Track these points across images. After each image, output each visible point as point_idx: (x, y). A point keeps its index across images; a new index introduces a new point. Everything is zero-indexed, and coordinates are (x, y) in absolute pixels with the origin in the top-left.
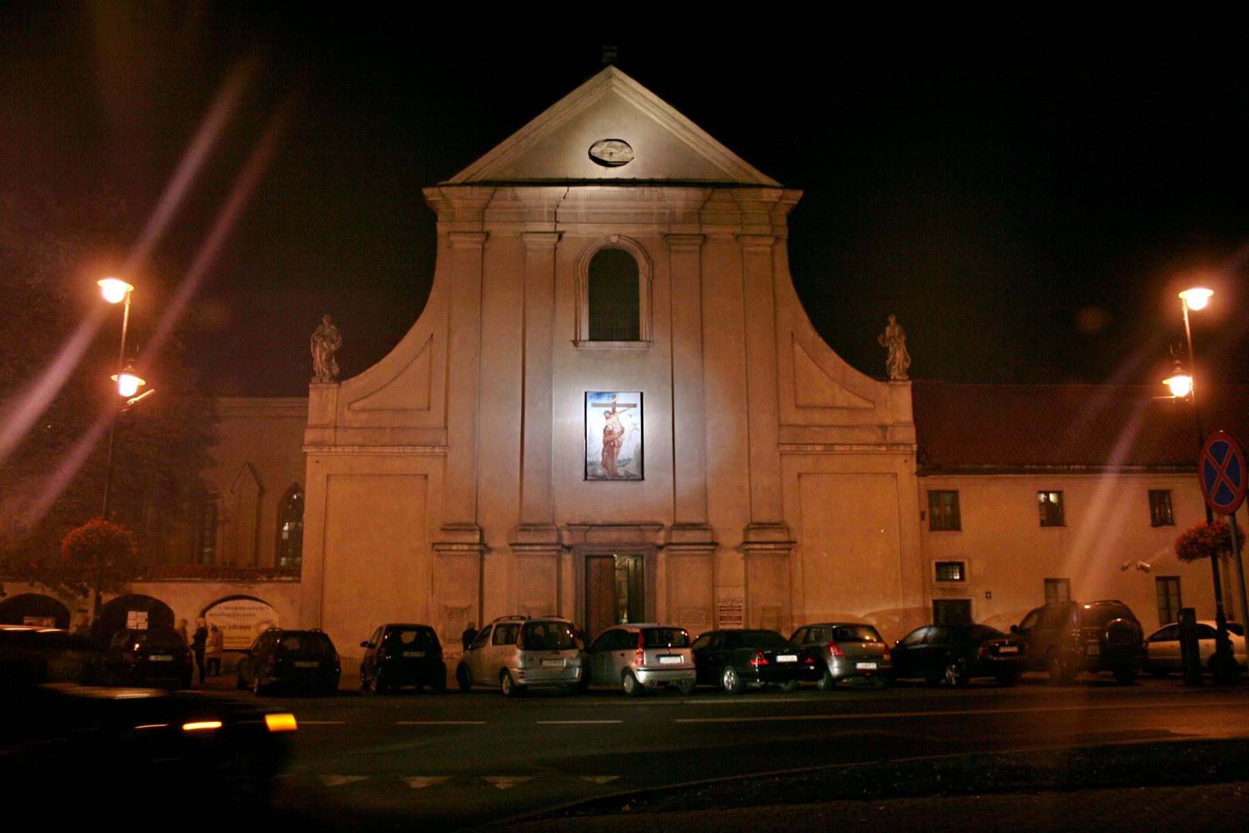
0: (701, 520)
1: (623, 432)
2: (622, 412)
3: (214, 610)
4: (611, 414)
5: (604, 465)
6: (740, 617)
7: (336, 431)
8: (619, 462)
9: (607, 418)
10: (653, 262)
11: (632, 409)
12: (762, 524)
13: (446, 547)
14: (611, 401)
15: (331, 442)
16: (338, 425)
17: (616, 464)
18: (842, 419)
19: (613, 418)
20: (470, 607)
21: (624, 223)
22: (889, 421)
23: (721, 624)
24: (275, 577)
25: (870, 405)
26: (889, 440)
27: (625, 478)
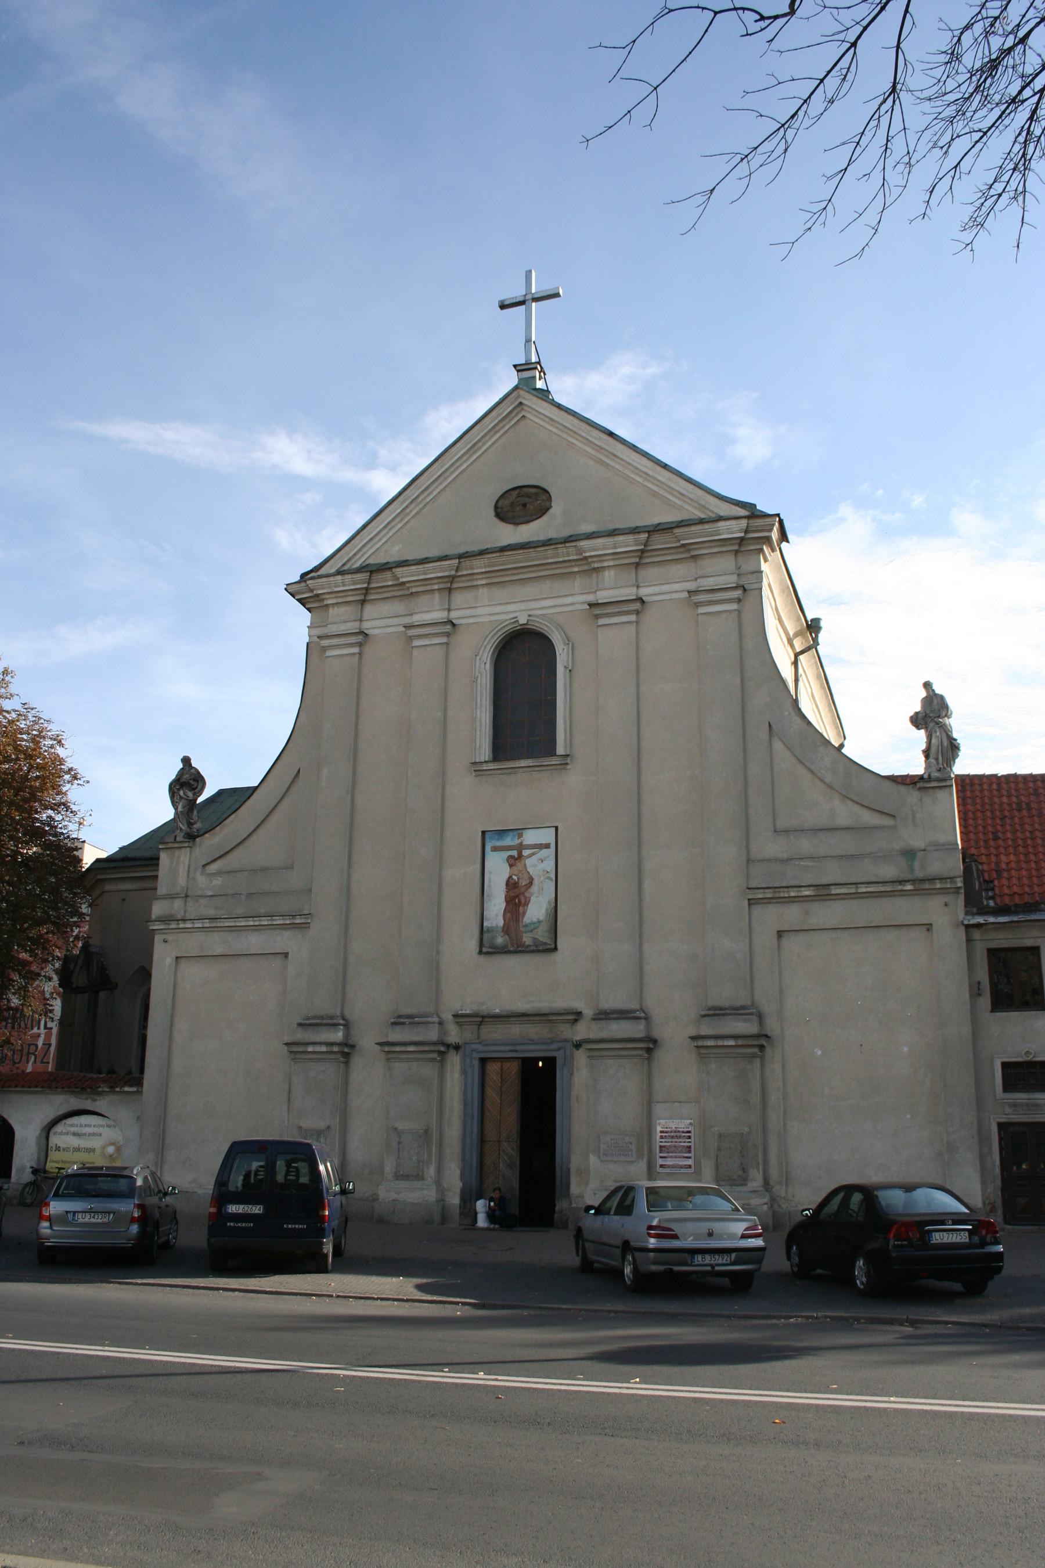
0: (633, 1005)
1: (531, 883)
2: (529, 856)
3: (59, 1128)
4: (517, 859)
5: (506, 930)
6: (690, 1147)
7: (186, 901)
8: (526, 926)
9: (511, 866)
10: (573, 644)
11: (545, 851)
12: (721, 1009)
13: (301, 1049)
14: (517, 842)
15: (179, 917)
16: (190, 893)
17: (522, 929)
18: (846, 844)
19: (519, 865)
20: (329, 1127)
22: (918, 843)
23: (661, 1157)
24: (117, 1087)
25: (888, 821)
26: (919, 874)
27: (532, 948)
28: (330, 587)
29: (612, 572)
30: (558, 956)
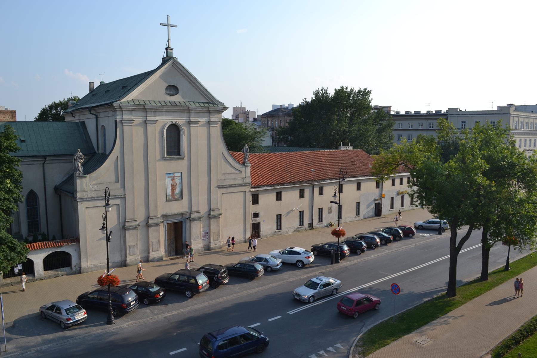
2: (176, 179)
4: (173, 179)
5: (172, 195)
19: (174, 181)
21: (190, 115)
28: (126, 106)
29: (193, 113)
30: (183, 200)
